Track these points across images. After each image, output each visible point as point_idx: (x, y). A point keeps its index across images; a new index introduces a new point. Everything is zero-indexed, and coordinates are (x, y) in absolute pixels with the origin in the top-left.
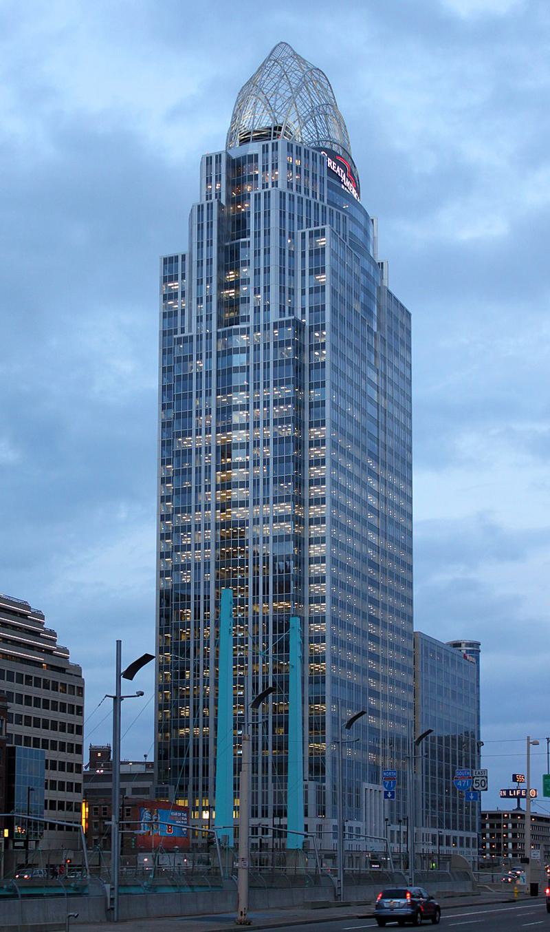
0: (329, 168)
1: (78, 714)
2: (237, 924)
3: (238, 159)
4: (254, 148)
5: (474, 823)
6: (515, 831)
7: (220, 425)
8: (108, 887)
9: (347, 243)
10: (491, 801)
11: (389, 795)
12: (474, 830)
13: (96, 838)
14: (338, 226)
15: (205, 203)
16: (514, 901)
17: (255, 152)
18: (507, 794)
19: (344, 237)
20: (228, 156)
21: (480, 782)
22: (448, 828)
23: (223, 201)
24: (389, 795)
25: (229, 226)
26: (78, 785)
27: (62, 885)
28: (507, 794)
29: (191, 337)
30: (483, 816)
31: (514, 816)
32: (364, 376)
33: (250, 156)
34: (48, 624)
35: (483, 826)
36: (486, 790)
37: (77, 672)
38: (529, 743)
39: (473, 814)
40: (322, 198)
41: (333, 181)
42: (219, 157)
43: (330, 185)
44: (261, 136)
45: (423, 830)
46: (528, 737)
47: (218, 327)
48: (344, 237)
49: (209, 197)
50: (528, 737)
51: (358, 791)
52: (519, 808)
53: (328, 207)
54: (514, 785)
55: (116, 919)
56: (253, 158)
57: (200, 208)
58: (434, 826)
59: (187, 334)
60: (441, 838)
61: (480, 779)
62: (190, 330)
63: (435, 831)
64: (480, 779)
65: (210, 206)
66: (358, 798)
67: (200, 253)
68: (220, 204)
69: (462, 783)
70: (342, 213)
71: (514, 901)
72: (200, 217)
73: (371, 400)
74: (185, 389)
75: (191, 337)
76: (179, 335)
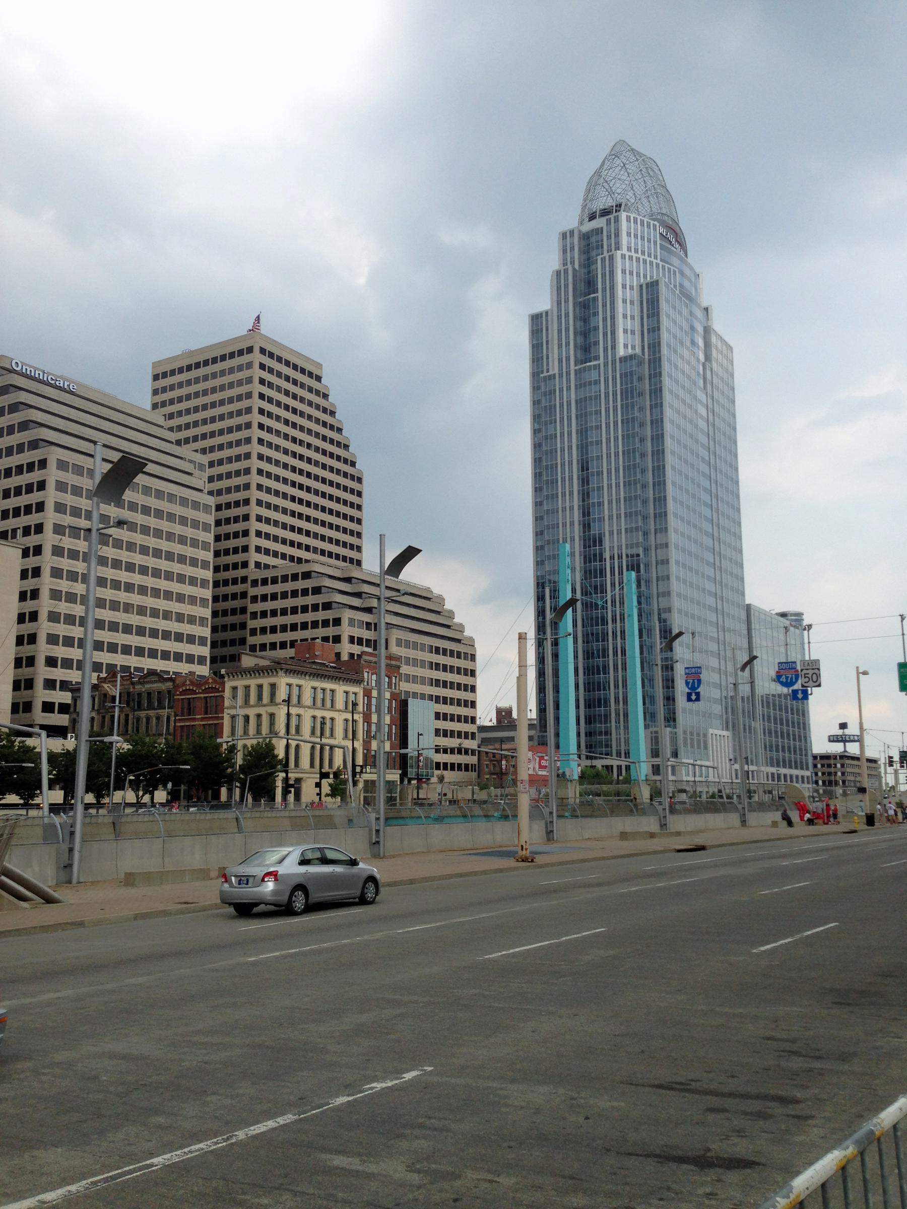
0: (661, 234)
1: (471, 676)
2: (518, 861)
3: (588, 233)
4: (600, 223)
5: (807, 764)
6: (843, 770)
7: (628, 526)
8: (373, 816)
9: (677, 292)
10: (820, 745)
11: (694, 697)
12: (807, 769)
13: (488, 776)
14: (669, 278)
15: (562, 269)
16: (855, 832)
17: (601, 225)
18: (833, 739)
19: (675, 286)
20: (580, 231)
21: (810, 676)
22: (784, 767)
23: (577, 266)
24: (694, 697)
25: (582, 287)
26: (473, 734)
27: (422, 815)
28: (833, 739)
29: (554, 375)
30: (815, 757)
31: (842, 757)
32: (695, 397)
33: (597, 229)
34: (448, 606)
35: (815, 766)
36: (819, 685)
37: (471, 643)
38: (858, 673)
39: (806, 755)
40: (656, 257)
41: (664, 243)
42: (572, 232)
43: (662, 247)
44: (605, 213)
45: (763, 768)
46: (857, 668)
47: (576, 365)
48: (675, 286)
49: (565, 264)
50: (857, 668)
51: (705, 735)
52: (845, 751)
53: (661, 263)
54: (840, 732)
55: (382, 855)
56: (599, 231)
57: (558, 273)
58: (772, 765)
59: (551, 373)
60: (779, 775)
61: (811, 672)
62: (553, 370)
63: (773, 770)
64: (811, 672)
65: (566, 271)
66: (705, 743)
67: (559, 310)
68: (574, 269)
69: (787, 678)
70: (672, 268)
71: (855, 832)
72: (559, 281)
73: (701, 402)
74: (551, 416)
75: (554, 375)
76: (545, 374)
